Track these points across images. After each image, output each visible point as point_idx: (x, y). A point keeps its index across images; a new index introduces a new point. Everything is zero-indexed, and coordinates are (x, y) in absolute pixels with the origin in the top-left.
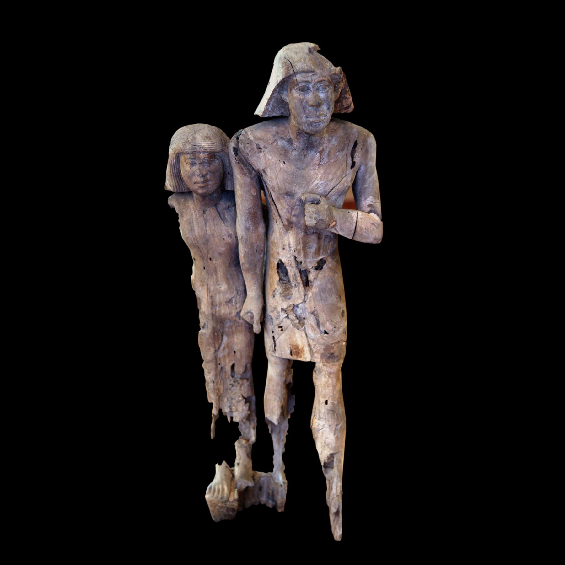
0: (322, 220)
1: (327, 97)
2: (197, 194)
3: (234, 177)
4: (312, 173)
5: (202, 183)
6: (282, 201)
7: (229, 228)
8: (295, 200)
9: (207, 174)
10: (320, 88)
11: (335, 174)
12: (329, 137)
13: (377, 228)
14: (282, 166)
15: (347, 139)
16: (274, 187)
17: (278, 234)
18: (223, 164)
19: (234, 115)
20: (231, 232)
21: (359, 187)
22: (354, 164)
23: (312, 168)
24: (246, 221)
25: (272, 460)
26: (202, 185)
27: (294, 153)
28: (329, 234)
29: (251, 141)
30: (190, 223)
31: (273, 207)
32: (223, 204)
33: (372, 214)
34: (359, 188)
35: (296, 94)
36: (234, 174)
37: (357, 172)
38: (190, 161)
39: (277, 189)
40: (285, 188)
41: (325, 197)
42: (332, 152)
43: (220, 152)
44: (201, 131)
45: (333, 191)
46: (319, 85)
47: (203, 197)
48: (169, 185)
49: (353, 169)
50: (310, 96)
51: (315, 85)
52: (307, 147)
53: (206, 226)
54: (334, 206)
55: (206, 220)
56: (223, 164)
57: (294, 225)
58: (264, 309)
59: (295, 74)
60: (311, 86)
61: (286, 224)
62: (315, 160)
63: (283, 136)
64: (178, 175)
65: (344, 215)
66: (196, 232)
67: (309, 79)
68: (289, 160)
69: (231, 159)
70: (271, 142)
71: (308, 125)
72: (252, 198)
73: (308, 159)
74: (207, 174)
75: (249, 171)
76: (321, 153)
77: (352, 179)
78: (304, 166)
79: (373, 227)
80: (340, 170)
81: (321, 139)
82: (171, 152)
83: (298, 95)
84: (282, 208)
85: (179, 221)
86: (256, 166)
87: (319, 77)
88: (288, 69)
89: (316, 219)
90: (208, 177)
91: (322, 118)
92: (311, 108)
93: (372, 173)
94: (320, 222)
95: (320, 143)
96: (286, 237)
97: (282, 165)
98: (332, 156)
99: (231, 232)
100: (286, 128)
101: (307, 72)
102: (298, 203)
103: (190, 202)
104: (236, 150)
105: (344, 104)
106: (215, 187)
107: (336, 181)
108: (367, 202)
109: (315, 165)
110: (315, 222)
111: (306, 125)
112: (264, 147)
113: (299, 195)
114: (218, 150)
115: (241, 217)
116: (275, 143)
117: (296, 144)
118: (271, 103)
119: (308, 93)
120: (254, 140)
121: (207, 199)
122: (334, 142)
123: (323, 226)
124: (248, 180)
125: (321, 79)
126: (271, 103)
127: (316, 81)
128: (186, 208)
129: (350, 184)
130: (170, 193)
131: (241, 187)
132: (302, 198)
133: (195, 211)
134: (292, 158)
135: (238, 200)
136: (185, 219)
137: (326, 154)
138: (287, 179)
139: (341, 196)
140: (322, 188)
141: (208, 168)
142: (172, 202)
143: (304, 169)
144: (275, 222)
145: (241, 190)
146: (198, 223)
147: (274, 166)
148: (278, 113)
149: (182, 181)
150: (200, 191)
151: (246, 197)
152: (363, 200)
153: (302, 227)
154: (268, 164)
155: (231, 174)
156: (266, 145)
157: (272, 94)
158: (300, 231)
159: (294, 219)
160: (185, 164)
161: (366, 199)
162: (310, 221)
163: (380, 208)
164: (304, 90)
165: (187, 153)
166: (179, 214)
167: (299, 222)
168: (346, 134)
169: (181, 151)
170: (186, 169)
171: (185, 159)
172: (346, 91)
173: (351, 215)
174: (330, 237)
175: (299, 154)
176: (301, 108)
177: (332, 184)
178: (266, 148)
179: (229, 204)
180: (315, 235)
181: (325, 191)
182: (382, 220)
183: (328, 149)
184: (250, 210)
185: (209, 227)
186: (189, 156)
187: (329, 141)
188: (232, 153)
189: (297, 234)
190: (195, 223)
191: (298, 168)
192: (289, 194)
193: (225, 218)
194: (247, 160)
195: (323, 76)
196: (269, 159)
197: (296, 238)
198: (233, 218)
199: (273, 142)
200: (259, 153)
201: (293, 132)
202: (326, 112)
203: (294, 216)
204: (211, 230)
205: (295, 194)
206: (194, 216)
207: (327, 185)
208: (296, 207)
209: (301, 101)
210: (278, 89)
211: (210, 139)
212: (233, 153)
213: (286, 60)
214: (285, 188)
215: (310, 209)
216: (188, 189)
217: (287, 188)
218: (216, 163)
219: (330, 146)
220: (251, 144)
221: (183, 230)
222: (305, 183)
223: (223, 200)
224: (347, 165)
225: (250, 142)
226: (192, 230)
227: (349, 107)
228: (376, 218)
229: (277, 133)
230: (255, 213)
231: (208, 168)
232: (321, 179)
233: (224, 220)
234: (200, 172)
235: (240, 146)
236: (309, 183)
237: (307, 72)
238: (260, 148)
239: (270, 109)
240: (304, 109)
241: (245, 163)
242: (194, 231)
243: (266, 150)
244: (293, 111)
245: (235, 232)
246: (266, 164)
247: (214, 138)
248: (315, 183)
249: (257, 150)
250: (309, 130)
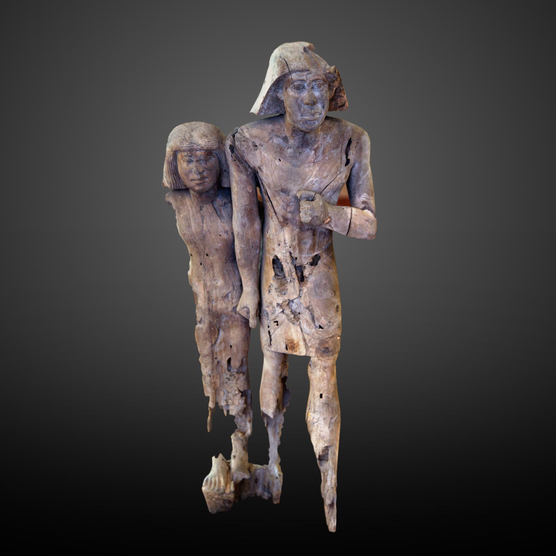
0: (317, 216)
1: (322, 96)
2: (194, 191)
3: (231, 174)
4: (307, 170)
5: (199, 180)
6: (278, 198)
7: (225, 224)
8: (290, 197)
9: (204, 171)
10: (315, 87)
11: (330, 171)
12: (324, 135)
13: (371, 224)
14: (277, 164)
15: (341, 136)
16: (270, 184)
17: (274, 231)
18: (220, 162)
20: (227, 228)
21: (353, 184)
22: (348, 161)
23: (307, 165)
24: (242, 217)
26: (199, 182)
27: (290, 151)
28: (324, 231)
29: (247, 139)
31: (268, 204)
32: (219, 201)
33: (366, 211)
34: (353, 185)
35: (291, 92)
36: (230, 171)
37: (351, 170)
38: (187, 158)
39: (272, 186)
40: (281, 185)
41: (320, 194)
42: (327, 150)
43: (216, 149)
44: (198, 129)
45: (328, 188)
46: (314, 83)
47: (200, 193)
48: (166, 181)
49: (347, 167)
50: (305, 95)
51: (309, 83)
52: (302, 145)
53: (203, 222)
54: (329, 203)
55: (203, 217)
56: (220, 162)
57: (289, 222)
59: (290, 72)
60: (306, 85)
61: (282, 220)
62: (310, 157)
63: (279, 134)
64: (174, 172)
65: (339, 212)
66: (193, 228)
67: (304, 78)
68: (285, 158)
69: (227, 156)
70: (267, 139)
71: (303, 123)
72: (248, 195)
73: (303, 156)
74: (204, 171)
75: (245, 168)
76: (316, 150)
77: (346, 176)
78: (299, 163)
79: (367, 223)
80: (335, 167)
81: (316, 137)
82: (168, 149)
83: (293, 93)
84: (277, 205)
86: (252, 163)
87: (314, 76)
88: (283, 68)
89: (311, 216)
90: (205, 174)
91: (317, 116)
92: (306, 106)
93: (366, 171)
94: (315, 219)
95: (315, 141)
96: (282, 234)
97: (277, 163)
98: (327, 154)
99: (227, 228)
100: (281, 126)
101: (302, 71)
102: (293, 200)
103: (187, 199)
104: (232, 148)
105: (339, 102)
106: (212, 184)
107: (331, 178)
108: (361, 198)
109: (310, 163)
110: (310, 218)
111: (301, 123)
112: (260, 144)
113: (295, 192)
114: (215, 147)
115: (237, 213)
116: (271, 141)
117: (291, 142)
118: (267, 101)
119: (303, 91)
120: (250, 138)
121: (204, 196)
122: (329, 140)
123: (318, 222)
124: (244, 177)
125: (316, 77)
126: (267, 101)
127: (311, 79)
128: (183, 204)
129: (345, 181)
131: (238, 184)
132: (297, 195)
133: (192, 208)
134: (287, 156)
135: (234, 197)
136: (182, 216)
137: (321, 152)
138: (283, 176)
139: (336, 193)
140: (317, 185)
141: (205, 166)
143: (299, 166)
144: (270, 218)
145: (237, 187)
146: (195, 219)
147: (270, 163)
149: (179, 178)
150: (197, 188)
151: (242, 194)
152: (357, 197)
153: (298, 223)
154: (264, 162)
155: (228, 171)
156: (262, 143)
157: (268, 93)
158: (295, 228)
159: (289, 216)
160: (182, 161)
161: (360, 196)
162: (305, 217)
164: (299, 88)
165: (184, 151)
167: (294, 219)
168: (341, 132)
169: (178, 149)
170: (183, 166)
171: (182, 157)
173: (346, 211)
174: (325, 233)
175: (295, 152)
176: (297, 107)
177: (326, 181)
178: (262, 146)
179: (225, 200)
180: (310, 231)
181: (320, 188)
183: (323, 147)
184: (246, 207)
185: (206, 223)
186: (186, 154)
187: (324, 139)
188: (228, 151)
189: (292, 230)
190: (192, 219)
191: (294, 166)
192: (285, 191)
193: (222, 215)
194: (243, 157)
195: (318, 75)
196: (264, 156)
197: (291, 234)
198: (229, 215)
199: (269, 140)
200: (254, 150)
201: (288, 129)
202: (321, 111)
203: (290, 212)
204: (207, 227)
205: (290, 191)
206: (191, 212)
207: (322, 182)
208: (291, 204)
209: (296, 99)
210: (273, 88)
211: (207, 137)
212: (229, 151)
213: (281, 59)
214: (281, 185)
215: (305, 206)
216: (185, 186)
217: (283, 185)
218: (213, 161)
219: (325, 143)
220: (247, 142)
221: (180, 226)
222: (300, 180)
223: (220, 197)
224: (341, 163)
225: (246, 140)
226: (189, 226)
229: (273, 131)
230: (251, 210)
231: (205, 166)
232: (316, 176)
233: (220, 216)
234: (197, 169)
235: (237, 143)
236: (304, 180)
237: (302, 71)
238: (256, 146)
239: (265, 107)
240: (299, 107)
241: (241, 161)
242: (191, 227)
243: (262, 148)
244: (288, 109)
245: (232, 229)
246: (262, 161)
247: (211, 136)
248: (310, 180)
249: (252, 148)
250: (304, 128)
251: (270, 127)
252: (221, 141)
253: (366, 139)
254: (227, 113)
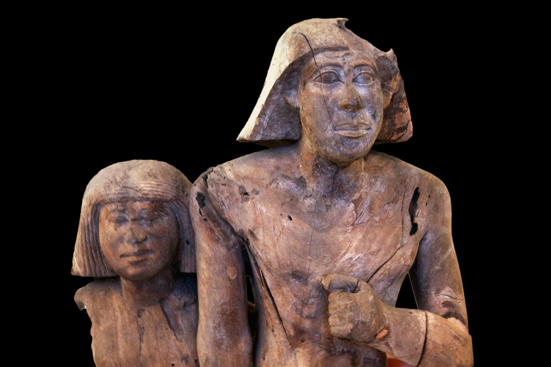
0: (363, 323)
1: (372, 96)
2: (126, 278)
3: (198, 247)
4: (341, 238)
5: (136, 254)
6: (285, 289)
7: (183, 344)
8: (310, 287)
9: (146, 239)
10: (360, 79)
11: (383, 242)
12: (370, 178)
13: (464, 345)
14: (285, 224)
15: (401, 183)
16: (270, 263)
17: (276, 355)
18: (178, 225)
19: (200, 137)
20: (187, 351)
22: (414, 228)
23: (340, 230)
24: (215, 328)
26: (134, 258)
27: (309, 202)
28: (372, 355)
29: (230, 181)
30: (111, 334)
31: (267, 303)
32: (175, 300)
33: (452, 320)
34: (425, 272)
35: (314, 88)
36: (197, 242)
37: (421, 243)
38: (116, 215)
39: (275, 265)
40: (292, 264)
41: (367, 282)
42: (377, 203)
43: (171, 200)
45: (380, 272)
46: (357, 72)
47: (138, 282)
48: (78, 265)
49: (413, 236)
50: (340, 91)
51: (349, 70)
52: (332, 192)
53: (141, 340)
54: (383, 301)
55: (141, 330)
56: (178, 225)
57: (306, 336)
58: (427, 328)
59: (314, 52)
60: (342, 74)
61: (292, 333)
62: (347, 215)
63: (288, 174)
64: (94, 248)
66: (121, 352)
67: (340, 61)
68: (300, 214)
69: (192, 214)
70: (266, 182)
71: (337, 143)
72: (228, 284)
73: (333, 213)
74: (146, 239)
75: (225, 234)
76: (357, 203)
77: (412, 252)
78: (326, 225)
79: (457, 342)
80: (391, 236)
81: (357, 179)
82: (85, 203)
83: (318, 90)
84: (284, 302)
85: (93, 332)
86: (238, 223)
87: (357, 58)
88: (300, 46)
89: (352, 321)
90: (148, 244)
91: (363, 131)
92: (341, 112)
93: (446, 247)
94: (360, 327)
95: (354, 186)
96: (291, 361)
97: (286, 223)
98: (377, 210)
99: (187, 351)
100: (293, 161)
101: (335, 49)
102: (314, 293)
103: (114, 297)
104: (202, 198)
105: (396, 122)
106: (160, 265)
107: (385, 255)
108: (441, 297)
109: (346, 225)
110: (351, 326)
111: (333, 143)
112: (254, 191)
113: (318, 278)
114: (170, 196)
115: (206, 320)
116: (274, 185)
117: (312, 186)
118: (268, 113)
119: (336, 86)
120: (235, 180)
121: (145, 288)
122: (380, 187)
123: (366, 336)
124: (223, 251)
125: (361, 61)
126: (268, 113)
127: (353, 64)
128: (106, 306)
131: (209, 264)
132: (323, 282)
133: (122, 313)
134: (304, 211)
135: (203, 289)
136: (102, 328)
137: (366, 206)
138: (295, 247)
140: (359, 266)
141: (149, 229)
142: (83, 298)
143: (326, 231)
144: (270, 331)
145: (208, 268)
146: (125, 334)
147: (272, 224)
148: (280, 132)
149: (102, 257)
150: (131, 271)
151: (216, 282)
152: (433, 293)
153: (323, 340)
154: (260, 220)
155: (192, 243)
156: (257, 188)
158: (317, 348)
159: (307, 324)
160: (107, 221)
161: (438, 291)
162: (339, 326)
163: (465, 309)
164: (330, 79)
165: (111, 202)
167: (316, 330)
168: (399, 175)
169: (100, 199)
170: (108, 230)
171: (108, 213)
172: (400, 97)
173: (416, 317)
174: (375, 360)
175: (318, 204)
176: (325, 112)
177: (377, 261)
178: (257, 193)
179: (186, 299)
180: (346, 356)
181: (365, 273)
182: (470, 332)
183: (369, 198)
184: (224, 307)
185: (147, 342)
186: (113, 207)
187: (371, 184)
188: (194, 203)
189: (312, 354)
190: (120, 335)
191: (315, 229)
192: (299, 276)
193: (178, 325)
194: (220, 213)
195: (365, 58)
196: (261, 212)
197: (310, 361)
198: (192, 326)
199: (270, 184)
200: (243, 201)
201: (306, 165)
202: (370, 126)
203: (308, 317)
204: (149, 349)
205: (309, 275)
206: (120, 321)
207: (369, 260)
208: (312, 300)
209: (325, 99)
210: (280, 87)
211: (155, 177)
212: (195, 203)
213: (295, 35)
214: (292, 264)
215: (338, 301)
216: (112, 271)
217: (295, 264)
218: (165, 222)
219: (373, 192)
220: (229, 186)
221: (97, 348)
222: (328, 256)
223: (176, 292)
224: (403, 228)
225: (228, 183)
226: (114, 347)
227: (404, 128)
228: (460, 327)
229: (277, 168)
230: (233, 314)
231: (149, 229)
232: (357, 250)
233: (174, 328)
234: (133, 234)
235: (210, 189)
236: (335, 256)
237: (335, 49)
238: (246, 194)
239: (265, 124)
240: (330, 113)
241: (218, 221)
242: (118, 349)
243: (257, 197)
244: (308, 120)
245: (195, 352)
246: (256, 221)
247: (163, 176)
248: (347, 256)
249: (239, 196)
250: (338, 153)
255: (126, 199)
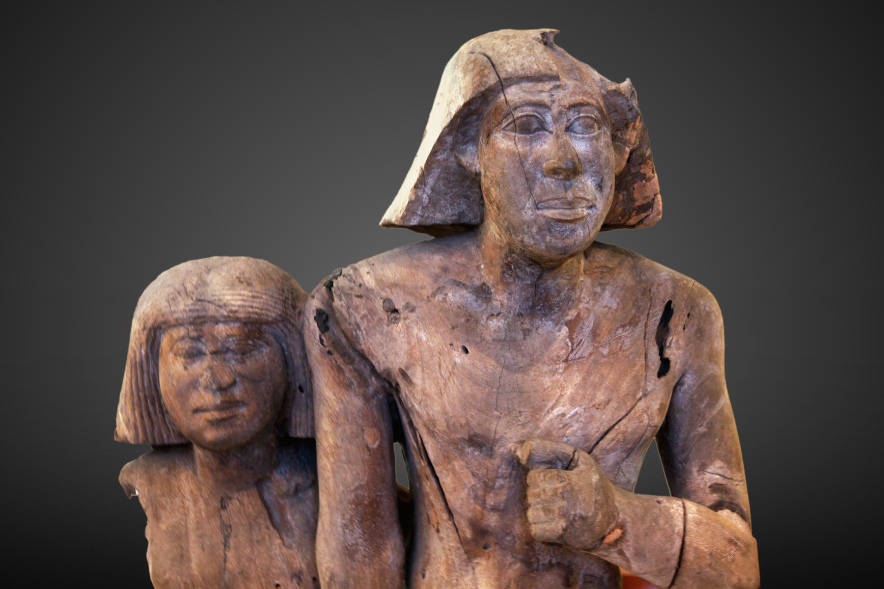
0: (583, 518)
1: (597, 154)
2: (203, 447)
3: (317, 397)
4: (547, 381)
5: (218, 408)
6: (457, 464)
7: (294, 552)
8: (497, 461)
9: (234, 383)
10: (577, 127)
11: (614, 388)
12: (593, 286)
13: (744, 554)
14: (458, 360)
15: (643, 294)
16: (433, 422)
17: (442, 569)
18: (286, 362)
20: (299, 563)
22: (665, 366)
23: (545, 369)
24: (345, 526)
25: (159, 273)
26: (216, 415)
27: (495, 324)
28: (597, 570)
29: (369, 290)
30: (178, 536)
31: (428, 486)
32: (281, 481)
33: (725, 513)
34: (681, 436)
35: (504, 142)
36: (316, 388)
37: (675, 389)
38: (185, 345)
39: (441, 426)
40: (468, 424)
41: (589, 453)
42: (605, 325)
43: (275, 322)
45: (609, 436)
46: (573, 115)
47: (222, 453)
48: (125, 424)
49: (663, 379)
50: (546, 147)
51: (560, 113)
52: (532, 308)
53: (226, 545)
54: (615, 483)
55: (226, 529)
56: (286, 362)
57: (491, 540)
59: (503, 84)
60: (549, 118)
61: (469, 534)
62: (556, 345)
63: (462, 279)
64: (151, 399)
65: (647, 510)
66: (194, 566)
67: (545, 97)
68: (481, 343)
69: (309, 344)
70: (426, 293)
71: (540, 229)
72: (366, 457)
73: (535, 341)
74: (234, 383)
75: (361, 375)
76: (572, 325)
77: (662, 405)
78: (523, 362)
79: (733, 550)
80: (628, 379)
81: (573, 288)
82: (136, 325)
83: (511, 144)
84: (456, 486)
85: (148, 533)
86: (382, 358)
87: (573, 93)
88: (481, 74)
89: (564, 515)
90: (238, 392)
91: (582, 211)
92: (548, 180)
93: (715, 396)
94: (577, 524)
95: (569, 299)
96: (468, 579)
97: (458, 357)
98: (604, 337)
99: (299, 563)
100: (470, 258)
101: (538, 78)
102: (504, 470)
103: (183, 476)
104: (324, 318)
105: (636, 195)
106: (256, 425)
107: (618, 409)
108: (708, 476)
109: (555, 361)
110: (563, 523)
111: (534, 230)
112: (407, 306)
113: (511, 446)
114: (272, 315)
115: (331, 514)
116: (440, 297)
117: (500, 298)
118: (431, 181)
119: (539, 138)
120: (376, 289)
121: (233, 462)
122: (609, 300)
123: (587, 538)
124: (358, 402)
125: (579, 98)
126: (431, 181)
127: (566, 102)
128: (171, 491)
130: (127, 451)
131: (336, 424)
132: (519, 453)
133: (195, 502)
134: (488, 338)
135: (325, 464)
136: (163, 527)
137: (587, 330)
138: (473, 396)
139: (633, 456)
140: (576, 426)
141: (239, 368)
142: (135, 478)
143: (523, 370)
144: (433, 530)
145: (334, 431)
146: (201, 536)
147: (436, 359)
148: (449, 212)
149: (164, 412)
150: (210, 435)
151: (347, 452)
152: (695, 470)
153: (518, 546)
154: (417, 353)
155: (308, 390)
156: (413, 302)
158: (509, 559)
159: (492, 520)
160: (171, 355)
161: (703, 468)
162: (544, 522)
164: (530, 127)
165: (179, 324)
166: (149, 513)
167: (506, 530)
168: (641, 282)
169: (160, 319)
170: (173, 369)
171: (173, 342)
172: (642, 156)
173: (668, 509)
174: (601, 579)
175: (509, 327)
176: (521, 180)
177: (605, 418)
178: (413, 310)
179: (298, 479)
180: (556, 571)
181: (586, 438)
183: (592, 318)
184: (360, 492)
185: (236, 548)
186: (182, 331)
187: (595, 296)
188: (312, 326)
189: (501, 568)
190: (192, 537)
191: (506, 367)
192: (480, 442)
193: (285, 522)
194: (353, 342)
195: (585, 93)
196: (419, 340)
197: (498, 579)
198: (308, 522)
199: (434, 295)
200: (390, 322)
201: (490, 264)
202: (593, 198)
203: (494, 509)
204: (239, 560)
205: (495, 441)
206: (192, 515)
207: (592, 418)
208: (500, 482)
209: (521, 159)
210: (449, 139)
211: (249, 284)
212: (314, 325)
213: (473, 57)
214: (468, 424)
215: (542, 484)
216: (180, 435)
217: (474, 423)
218: (264, 355)
219: (598, 309)
220: (368, 298)
221: (155, 558)
222: (527, 411)
223: (282, 469)
224: (646, 367)
225: (365, 294)
226: (182, 557)
228: (736, 524)
229: (445, 270)
230: (375, 503)
231: (239, 368)
232: (573, 401)
233: (280, 527)
234: (213, 375)
235: (337, 303)
236: (537, 411)
237: (538, 78)
238: (395, 311)
239: (425, 199)
240: (530, 181)
241: (350, 354)
242: (189, 560)
243: (413, 316)
244: (494, 192)
245: (313, 565)
246: (410, 354)
247: (261, 283)
248: (556, 412)
249: (383, 315)
250: (543, 246)
251: (436, 260)
252: (291, 303)
253: (711, 304)
254: (312, 232)
255: (202, 320)
